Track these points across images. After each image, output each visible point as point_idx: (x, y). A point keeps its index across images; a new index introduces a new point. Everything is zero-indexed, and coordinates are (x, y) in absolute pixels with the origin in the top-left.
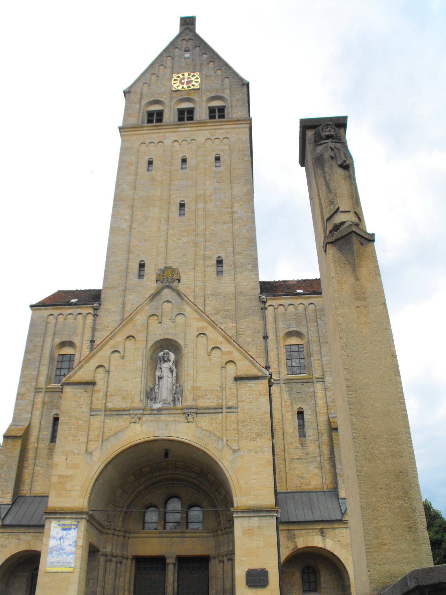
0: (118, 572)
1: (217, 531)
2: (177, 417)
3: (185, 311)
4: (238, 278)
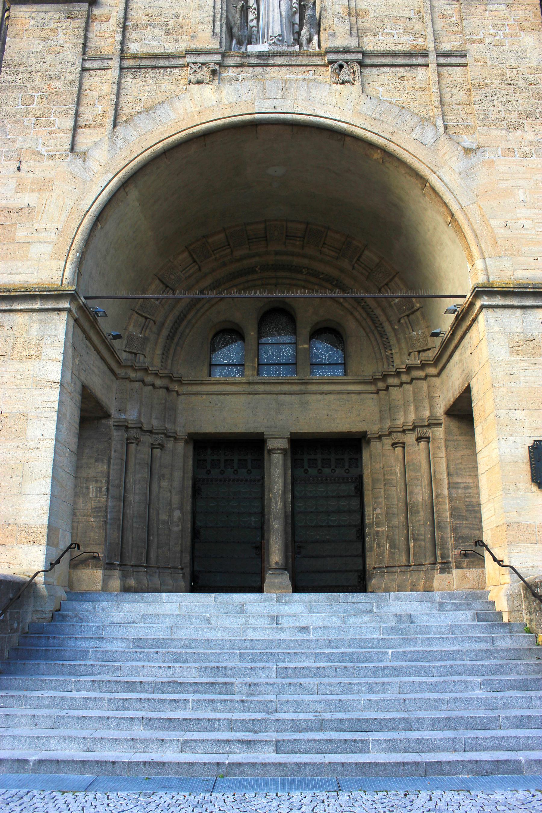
0: (156, 466)
1: (385, 377)
2: (311, 73)
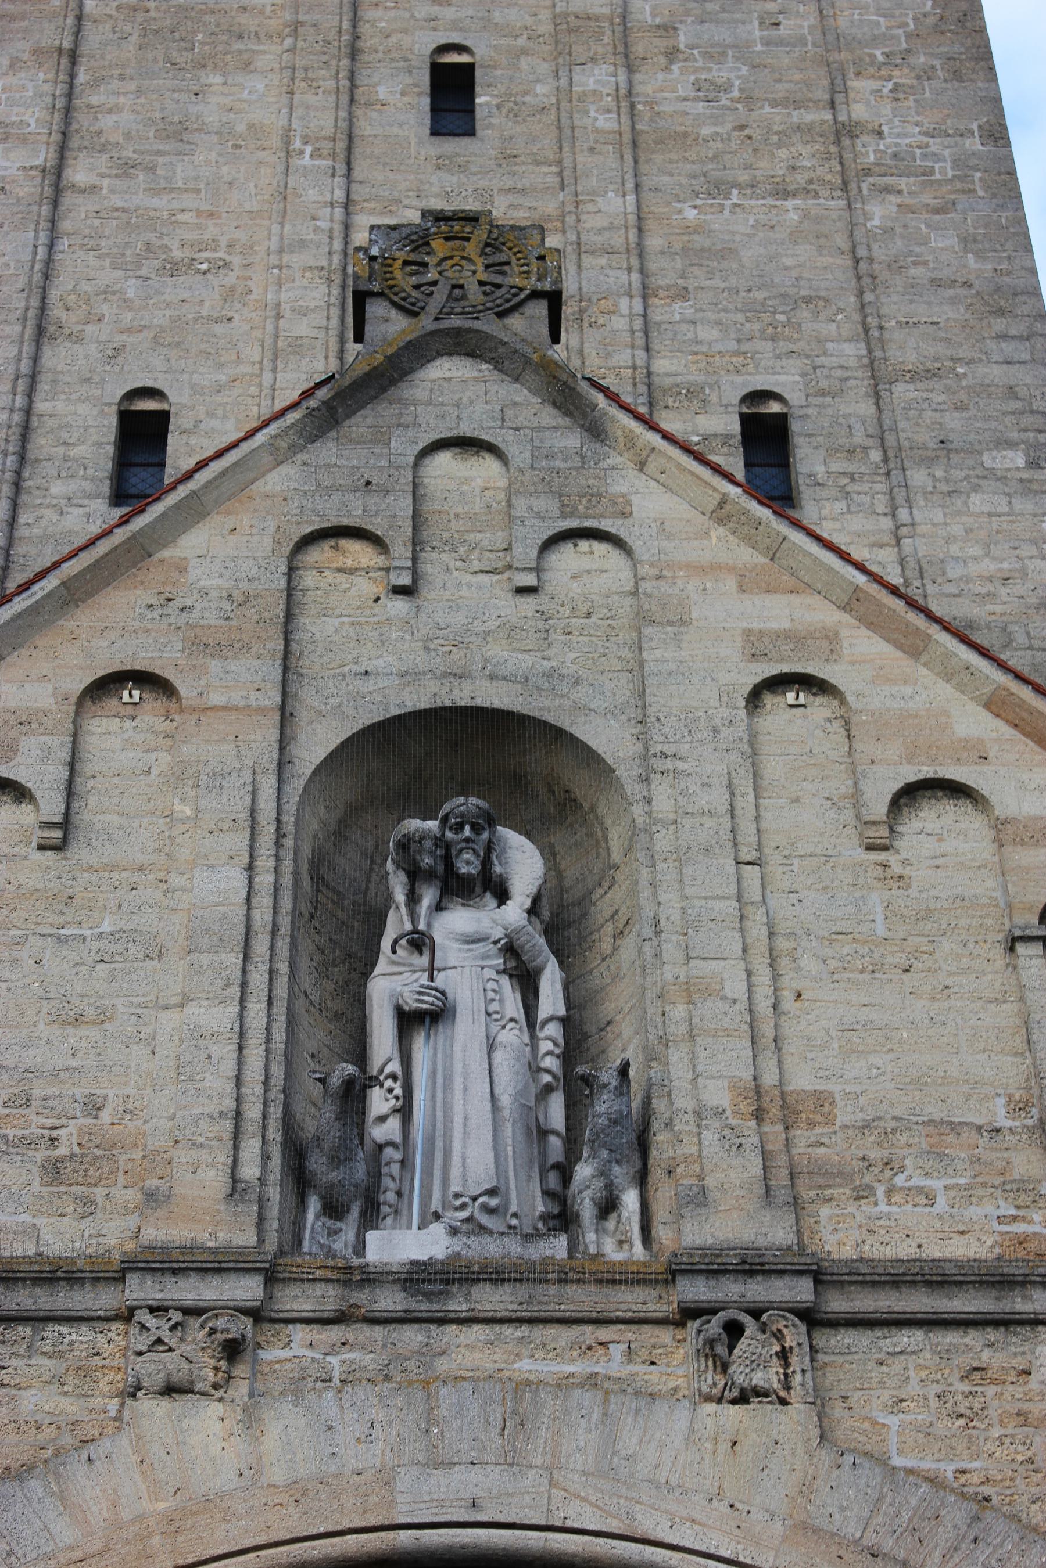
2: (617, 1351)
3: (625, 515)
4: (921, 529)
